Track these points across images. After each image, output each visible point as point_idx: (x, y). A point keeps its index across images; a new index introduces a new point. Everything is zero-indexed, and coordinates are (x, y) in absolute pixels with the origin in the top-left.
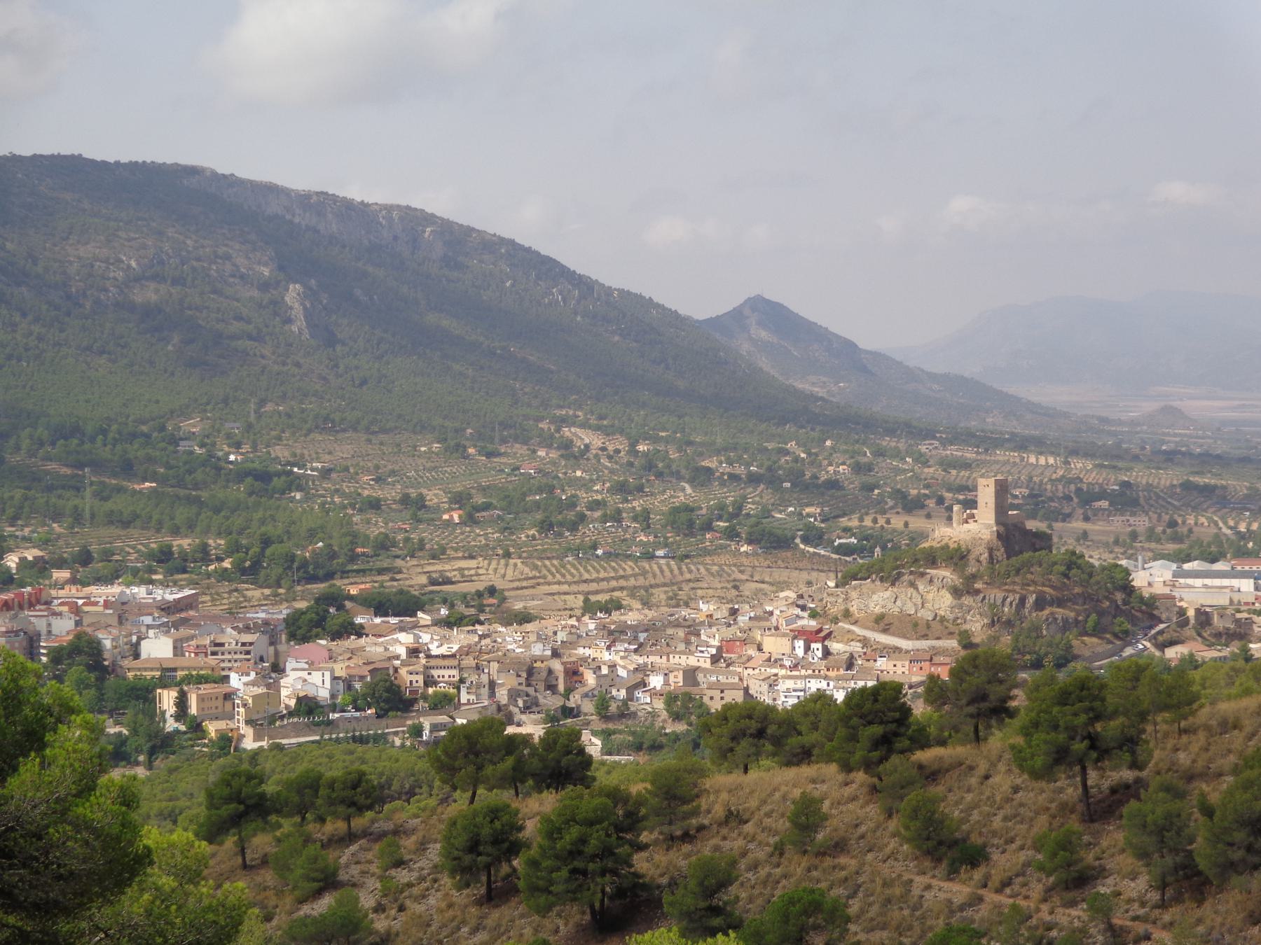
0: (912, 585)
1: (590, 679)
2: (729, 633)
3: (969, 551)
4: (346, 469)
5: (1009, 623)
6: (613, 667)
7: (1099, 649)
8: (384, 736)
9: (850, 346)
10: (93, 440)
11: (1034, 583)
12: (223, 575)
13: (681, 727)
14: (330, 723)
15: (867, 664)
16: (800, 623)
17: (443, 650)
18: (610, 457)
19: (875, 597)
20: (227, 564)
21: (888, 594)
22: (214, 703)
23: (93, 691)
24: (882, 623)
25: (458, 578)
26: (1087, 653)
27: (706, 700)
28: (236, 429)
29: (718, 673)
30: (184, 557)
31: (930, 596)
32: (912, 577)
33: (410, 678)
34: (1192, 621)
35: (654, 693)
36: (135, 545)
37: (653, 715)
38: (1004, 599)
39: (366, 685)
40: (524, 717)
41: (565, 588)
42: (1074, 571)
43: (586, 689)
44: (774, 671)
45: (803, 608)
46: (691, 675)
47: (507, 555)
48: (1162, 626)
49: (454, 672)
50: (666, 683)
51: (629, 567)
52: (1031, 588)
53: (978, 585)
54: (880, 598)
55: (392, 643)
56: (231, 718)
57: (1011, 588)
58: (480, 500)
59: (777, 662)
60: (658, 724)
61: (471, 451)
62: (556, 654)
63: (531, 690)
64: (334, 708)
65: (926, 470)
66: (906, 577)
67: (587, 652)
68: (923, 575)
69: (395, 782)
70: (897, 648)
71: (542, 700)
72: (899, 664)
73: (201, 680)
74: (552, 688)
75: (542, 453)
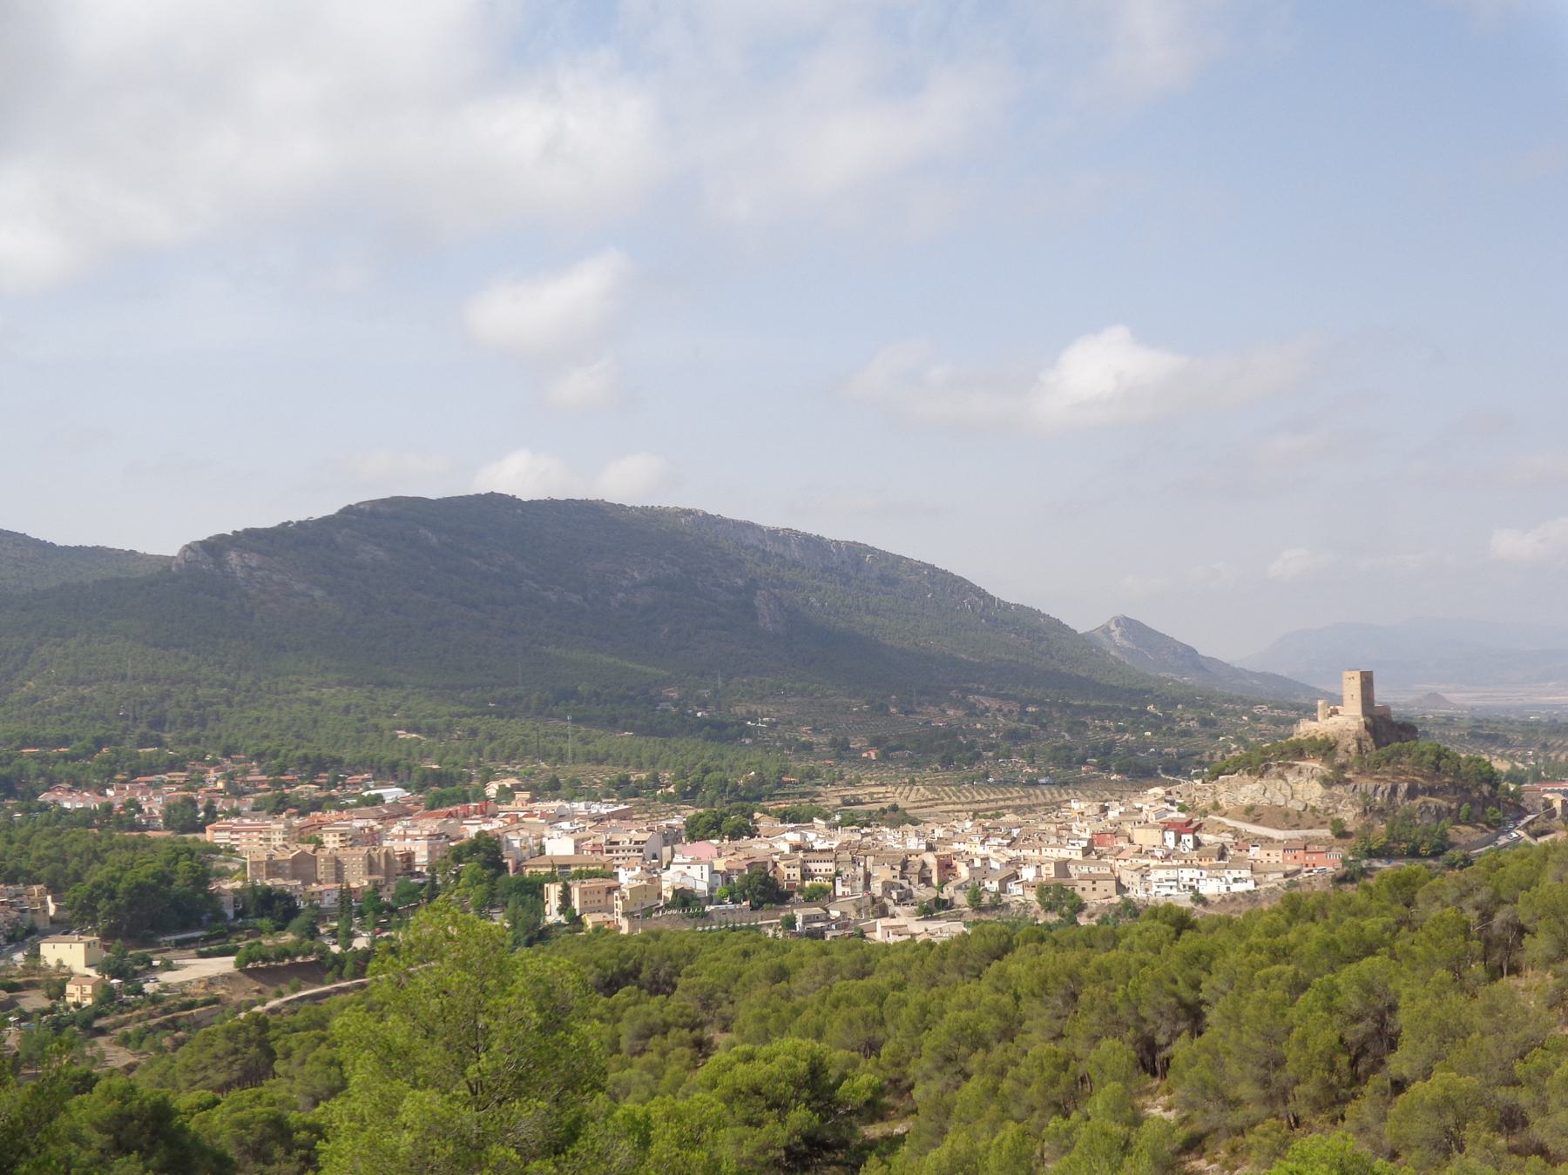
0: (1281, 776)
1: (963, 872)
2: (1099, 827)
3: (1337, 743)
4: (790, 723)
5: (1381, 811)
6: (985, 859)
7: (1474, 838)
8: (757, 928)
9: (1192, 651)
11: (1405, 773)
12: (668, 798)
13: (1053, 918)
14: (706, 915)
15: (1239, 854)
16: (1170, 816)
17: (825, 846)
18: (1005, 716)
19: (1243, 790)
20: (671, 790)
21: (1256, 786)
23: (485, 886)
24: (1252, 814)
25: (868, 799)
26: (1463, 842)
27: (1078, 891)
28: (706, 693)
29: (1090, 864)
30: (640, 785)
31: (1300, 787)
33: (789, 873)
34: (1559, 812)
35: (1027, 885)
36: (602, 776)
37: (1026, 906)
38: (1376, 788)
40: (898, 909)
41: (959, 807)
43: (959, 882)
44: (1145, 862)
45: (1172, 803)
46: (1062, 867)
47: (913, 782)
49: (831, 866)
50: (1039, 875)
51: (1016, 792)
54: (1248, 791)
55: (776, 843)
56: (611, 912)
58: (893, 743)
59: (1149, 853)
60: (1031, 915)
61: (893, 710)
62: (930, 848)
63: (905, 883)
64: (710, 901)
67: (962, 847)
68: (1291, 766)
69: (644, 968)
71: (915, 893)
72: (1272, 853)
73: (580, 875)
74: (926, 880)
75: (951, 712)
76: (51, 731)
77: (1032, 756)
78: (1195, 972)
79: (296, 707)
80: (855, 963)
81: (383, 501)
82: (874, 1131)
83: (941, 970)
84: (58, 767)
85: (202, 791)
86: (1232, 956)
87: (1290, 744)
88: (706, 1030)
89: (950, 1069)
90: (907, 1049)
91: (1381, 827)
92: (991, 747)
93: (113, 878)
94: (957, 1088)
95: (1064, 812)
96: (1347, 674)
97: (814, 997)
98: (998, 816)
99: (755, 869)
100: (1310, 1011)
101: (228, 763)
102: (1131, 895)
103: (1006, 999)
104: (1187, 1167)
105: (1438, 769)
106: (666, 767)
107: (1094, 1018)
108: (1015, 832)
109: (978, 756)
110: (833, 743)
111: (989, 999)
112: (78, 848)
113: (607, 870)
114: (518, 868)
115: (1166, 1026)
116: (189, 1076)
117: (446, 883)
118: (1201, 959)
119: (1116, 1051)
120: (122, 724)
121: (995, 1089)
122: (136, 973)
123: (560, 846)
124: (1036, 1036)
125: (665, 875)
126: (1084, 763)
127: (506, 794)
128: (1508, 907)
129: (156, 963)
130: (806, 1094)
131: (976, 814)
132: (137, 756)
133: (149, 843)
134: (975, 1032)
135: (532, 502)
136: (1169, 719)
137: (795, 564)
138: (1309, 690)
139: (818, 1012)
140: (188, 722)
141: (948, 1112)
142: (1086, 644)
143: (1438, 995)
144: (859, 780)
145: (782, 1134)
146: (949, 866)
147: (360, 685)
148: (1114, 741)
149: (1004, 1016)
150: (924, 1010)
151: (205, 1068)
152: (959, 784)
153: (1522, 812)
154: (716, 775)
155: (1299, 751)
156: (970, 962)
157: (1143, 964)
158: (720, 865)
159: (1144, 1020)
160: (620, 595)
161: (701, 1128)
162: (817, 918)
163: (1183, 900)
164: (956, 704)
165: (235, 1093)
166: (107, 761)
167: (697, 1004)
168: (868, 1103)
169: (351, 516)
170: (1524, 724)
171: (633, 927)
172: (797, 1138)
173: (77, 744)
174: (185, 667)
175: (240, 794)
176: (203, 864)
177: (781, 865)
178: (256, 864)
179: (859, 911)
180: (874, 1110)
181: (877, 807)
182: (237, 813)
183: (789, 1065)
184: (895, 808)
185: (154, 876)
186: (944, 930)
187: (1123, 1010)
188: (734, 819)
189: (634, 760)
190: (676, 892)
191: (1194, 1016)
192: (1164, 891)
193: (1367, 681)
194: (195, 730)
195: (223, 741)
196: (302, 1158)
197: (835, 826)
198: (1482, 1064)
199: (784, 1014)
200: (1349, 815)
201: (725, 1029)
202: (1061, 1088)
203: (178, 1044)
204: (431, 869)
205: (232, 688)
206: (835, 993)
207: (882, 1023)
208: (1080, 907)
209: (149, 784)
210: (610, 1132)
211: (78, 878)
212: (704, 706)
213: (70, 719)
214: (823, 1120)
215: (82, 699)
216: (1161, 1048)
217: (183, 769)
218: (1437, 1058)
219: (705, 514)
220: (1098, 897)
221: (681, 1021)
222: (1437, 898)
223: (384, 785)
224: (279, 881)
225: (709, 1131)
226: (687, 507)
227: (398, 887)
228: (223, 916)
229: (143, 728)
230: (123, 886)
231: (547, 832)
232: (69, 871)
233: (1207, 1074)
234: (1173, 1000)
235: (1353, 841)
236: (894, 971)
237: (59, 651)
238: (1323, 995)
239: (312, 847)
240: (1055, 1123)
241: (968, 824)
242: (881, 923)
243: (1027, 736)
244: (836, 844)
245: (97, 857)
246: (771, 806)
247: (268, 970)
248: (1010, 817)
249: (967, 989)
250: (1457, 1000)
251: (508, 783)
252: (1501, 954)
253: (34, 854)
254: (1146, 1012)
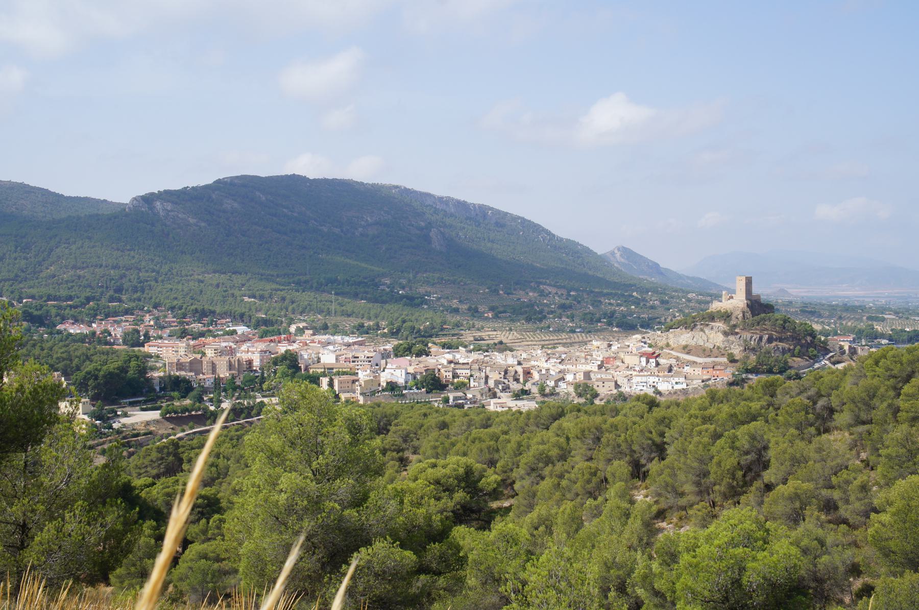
0: (702, 330)
1: (536, 376)
2: (607, 355)
5: (753, 349)
6: (548, 370)
7: (802, 364)
8: (429, 402)
10: (343, 284)
11: (767, 330)
12: (384, 335)
13: (582, 400)
14: (403, 395)
20: (386, 331)
22: (347, 385)
24: (686, 349)
26: (796, 366)
27: (595, 387)
28: (404, 282)
30: (369, 328)
31: (711, 336)
33: (446, 375)
34: (847, 352)
35: (569, 383)
37: (568, 394)
39: (422, 377)
44: (630, 373)
45: (645, 343)
46: (587, 374)
47: (511, 330)
48: (831, 354)
49: (468, 371)
50: (575, 378)
51: (564, 335)
54: (684, 337)
55: (439, 360)
56: (354, 392)
58: (501, 309)
60: (570, 399)
62: (519, 363)
63: (506, 381)
68: (707, 325)
70: (694, 362)
71: (511, 386)
73: (338, 373)
74: (517, 380)
75: (531, 294)
76: (63, 293)
77: (573, 317)
78: (662, 428)
79: (191, 283)
80: (482, 420)
81: (237, 177)
82: (495, 505)
83: (527, 425)
84: (67, 311)
85: (142, 326)
86: (682, 420)
87: (708, 314)
88: (406, 452)
89: (534, 474)
90: (510, 464)
91: (753, 358)
92: (552, 312)
93: (96, 369)
94: (537, 484)
95: (589, 347)
96: (739, 278)
97: (462, 438)
98: (554, 348)
99: (429, 372)
100: (723, 448)
101: (155, 311)
102: (622, 389)
103: (562, 440)
104: (656, 525)
105: (784, 328)
106: (383, 319)
107: (609, 450)
108: (563, 356)
109: (545, 317)
110: (469, 309)
111: (554, 439)
112: (78, 353)
113: (353, 371)
114: (307, 369)
115: (646, 455)
116: (138, 471)
117: (269, 376)
118: (666, 422)
119: (621, 467)
120: (100, 290)
121: (559, 484)
122: (109, 418)
123: (328, 358)
124: (577, 458)
125: (382, 374)
126: (600, 321)
127: (301, 331)
128: (825, 399)
129: (119, 413)
130: (463, 485)
131: (543, 347)
132: (108, 307)
133: (114, 352)
134: (547, 456)
135: (314, 180)
136: (644, 300)
137: (452, 215)
138: (716, 285)
139: (464, 445)
140: (135, 290)
141: (534, 495)
142: (602, 260)
143: (790, 441)
144: (483, 328)
145: (451, 504)
146: (529, 373)
147: (224, 273)
148: (615, 311)
149: (561, 448)
150: (519, 445)
151: (146, 467)
152: (534, 331)
153: (827, 351)
154: (408, 324)
155: (712, 318)
156: (542, 421)
157: (635, 423)
158: (411, 370)
159: (635, 452)
160: (360, 229)
161: (422, 498)
162: (460, 398)
163: (650, 392)
164: (534, 290)
165: (163, 479)
166: (93, 309)
167: (401, 440)
168: (495, 489)
169: (219, 184)
170: (829, 306)
171: (365, 401)
172: (458, 507)
173: (76, 300)
174: (133, 261)
175: (162, 328)
176: (144, 363)
177: (442, 371)
178: (171, 364)
179: (482, 395)
180: (495, 494)
181: (491, 342)
182: (161, 338)
183: (455, 470)
184: (501, 343)
185: (118, 368)
186: (527, 405)
187: (624, 446)
188: (419, 346)
189: (366, 316)
190: (388, 383)
191: (660, 450)
192: (640, 388)
193: (749, 282)
194: (139, 294)
195: (153, 300)
196: (199, 512)
197: (470, 351)
198: (814, 477)
199: (447, 445)
200: (737, 351)
201: (415, 453)
202: (593, 485)
203: (131, 455)
204: (262, 369)
205: (158, 272)
206: (473, 435)
207: (498, 450)
208: (596, 395)
209: (115, 321)
210: (385, 496)
211: (78, 368)
212: (403, 288)
213: (72, 287)
214: (471, 498)
215: (79, 277)
216: (644, 466)
217: (133, 314)
218: (790, 474)
219: (405, 188)
220: (605, 390)
221: (393, 448)
222: (787, 393)
223: (237, 325)
224: (183, 373)
225: (426, 499)
226: (396, 184)
227: (244, 377)
228: (155, 390)
229: (111, 293)
230: (102, 373)
231: (321, 351)
232: (74, 365)
233: (668, 479)
234: (650, 442)
235: (738, 364)
236: (503, 425)
237: (67, 251)
238: (729, 441)
239: (200, 356)
240: (590, 502)
241: (539, 352)
242: (493, 401)
243: (570, 307)
244: (470, 360)
245: (88, 358)
246: (437, 340)
247: (177, 418)
248: (560, 349)
249: (542, 434)
250: (800, 444)
251: (301, 325)
252: (823, 421)
253: (55, 356)
254: (635, 447)
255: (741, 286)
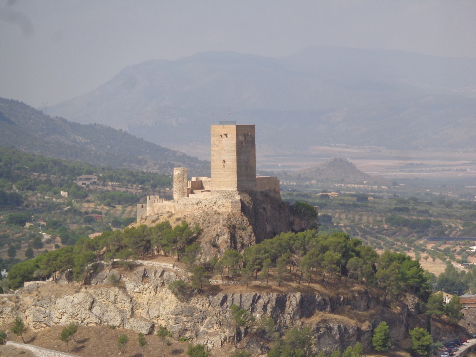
0: (116, 282)
3: (200, 232)
5: (261, 334)
19: (61, 302)
21: (80, 297)
31: (144, 299)
32: (115, 271)
38: (255, 301)
42: (353, 260)
52: (294, 285)
53: (216, 281)
57: (264, 284)
65: (86, 205)
66: (107, 272)
68: (131, 267)
87: (131, 233)
96: (218, 129)
105: (344, 271)
155: (144, 244)
170: (465, 205)
190: (26, 256)
193: (246, 141)
255: (223, 151)
